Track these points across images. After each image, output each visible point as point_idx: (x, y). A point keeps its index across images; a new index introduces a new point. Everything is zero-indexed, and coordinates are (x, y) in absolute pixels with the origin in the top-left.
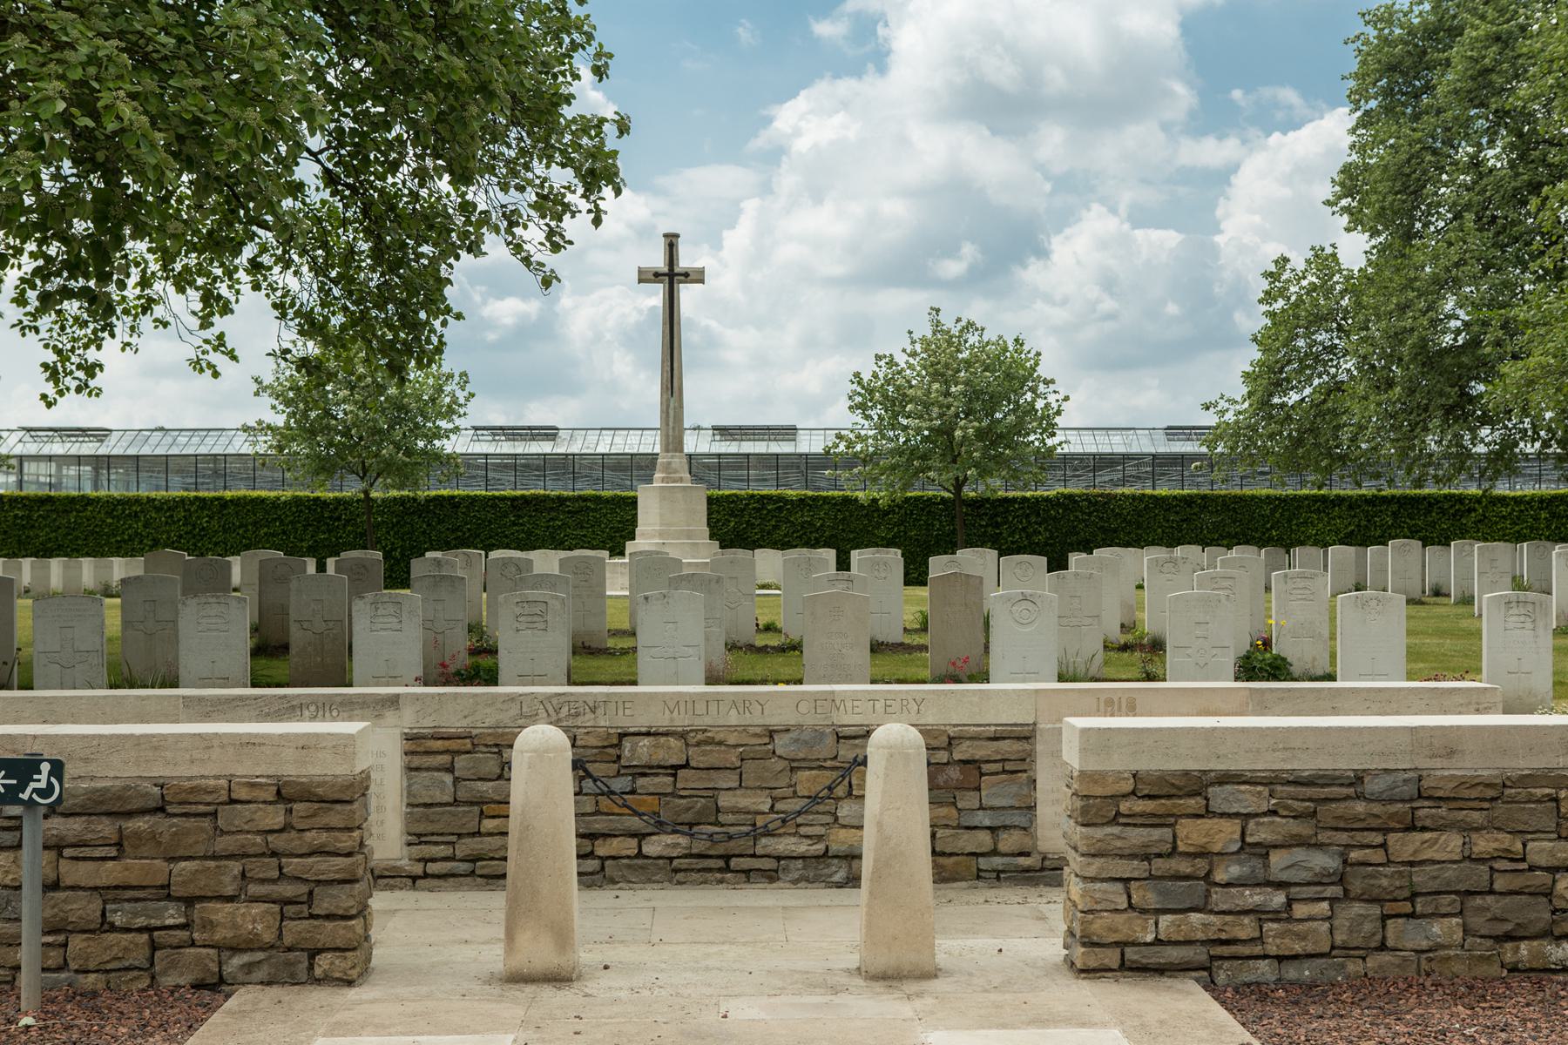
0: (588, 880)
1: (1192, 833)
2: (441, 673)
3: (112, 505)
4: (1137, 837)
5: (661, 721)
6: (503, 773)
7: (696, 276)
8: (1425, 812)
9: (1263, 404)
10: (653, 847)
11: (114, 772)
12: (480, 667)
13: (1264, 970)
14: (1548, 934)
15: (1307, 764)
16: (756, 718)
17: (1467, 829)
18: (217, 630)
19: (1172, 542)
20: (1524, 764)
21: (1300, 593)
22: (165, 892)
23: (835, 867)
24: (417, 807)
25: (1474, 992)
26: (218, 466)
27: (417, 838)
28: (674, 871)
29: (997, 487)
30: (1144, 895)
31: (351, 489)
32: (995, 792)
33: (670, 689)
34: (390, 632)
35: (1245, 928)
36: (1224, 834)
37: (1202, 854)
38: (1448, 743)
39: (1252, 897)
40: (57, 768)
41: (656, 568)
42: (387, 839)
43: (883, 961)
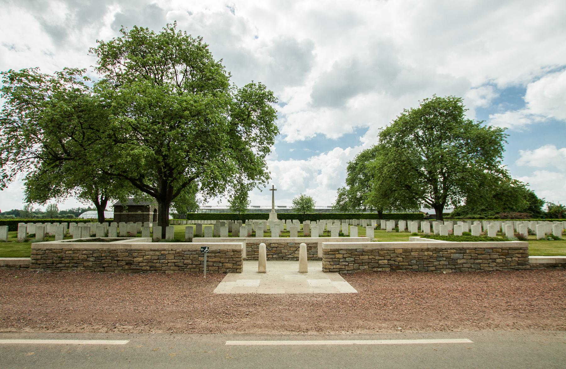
0: (268, 260)
1: (337, 256)
2: (250, 236)
3: (212, 214)
4: (331, 256)
5: (275, 242)
6: (258, 248)
7: (276, 190)
8: (364, 253)
9: (337, 204)
10: (274, 256)
11: (214, 248)
12: (253, 235)
13: (346, 272)
14: (378, 267)
15: (350, 248)
16: (286, 242)
17: (368, 255)
18: (224, 231)
19: (328, 219)
20: (375, 248)
21: (345, 226)
22: (220, 262)
23: (297, 259)
24: (248, 252)
25: (370, 274)
26: (223, 210)
27: (247, 255)
28: (276, 259)
29: (308, 213)
30: (332, 263)
31: (238, 213)
32: (313, 250)
33: (275, 238)
34: (244, 229)
35: (344, 267)
36: (341, 256)
37: (339, 258)
38: (366, 245)
39: (344, 263)
40: (208, 248)
41: (272, 222)
42: (244, 255)
43: (302, 271)
